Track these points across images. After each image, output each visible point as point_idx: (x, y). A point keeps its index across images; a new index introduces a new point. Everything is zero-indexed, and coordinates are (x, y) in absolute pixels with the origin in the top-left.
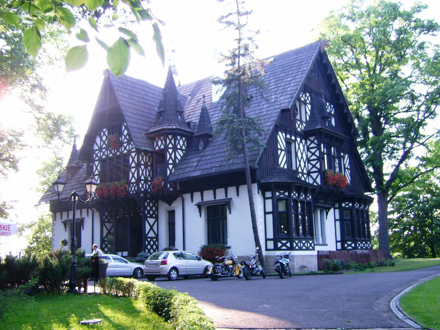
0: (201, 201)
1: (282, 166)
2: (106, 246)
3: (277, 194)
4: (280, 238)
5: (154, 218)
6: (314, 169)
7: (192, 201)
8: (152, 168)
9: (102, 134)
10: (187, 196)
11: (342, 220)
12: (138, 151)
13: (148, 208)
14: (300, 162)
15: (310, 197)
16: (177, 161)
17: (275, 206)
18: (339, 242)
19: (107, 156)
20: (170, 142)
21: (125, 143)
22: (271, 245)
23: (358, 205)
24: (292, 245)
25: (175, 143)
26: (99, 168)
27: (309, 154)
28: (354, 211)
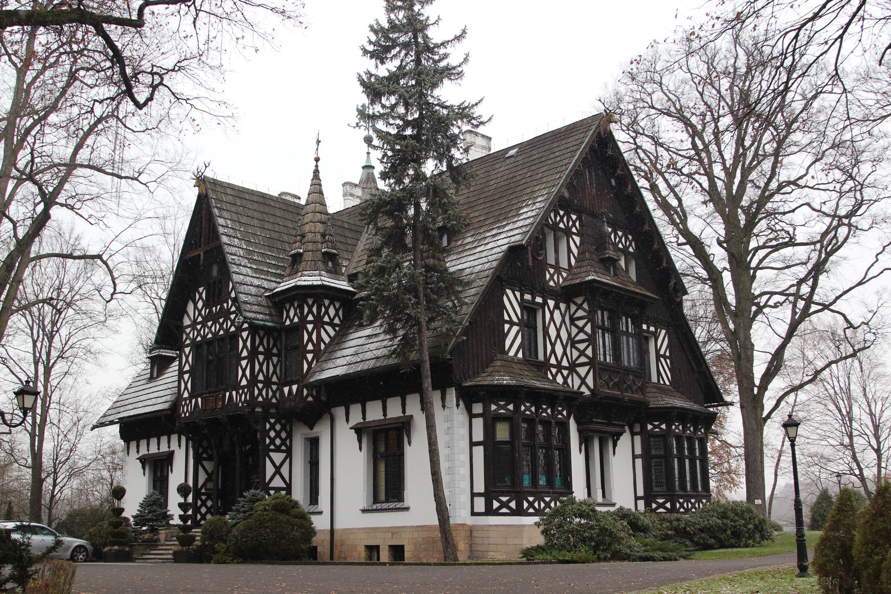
1: (512, 353)
2: (204, 503)
3: (493, 407)
4: (495, 492)
5: (283, 451)
7: (347, 420)
9: (197, 296)
10: (340, 412)
11: (646, 456)
12: (254, 329)
13: (272, 434)
14: (553, 345)
16: (323, 346)
17: (489, 430)
18: (640, 498)
19: (215, 334)
20: (310, 311)
22: (480, 504)
24: (519, 505)
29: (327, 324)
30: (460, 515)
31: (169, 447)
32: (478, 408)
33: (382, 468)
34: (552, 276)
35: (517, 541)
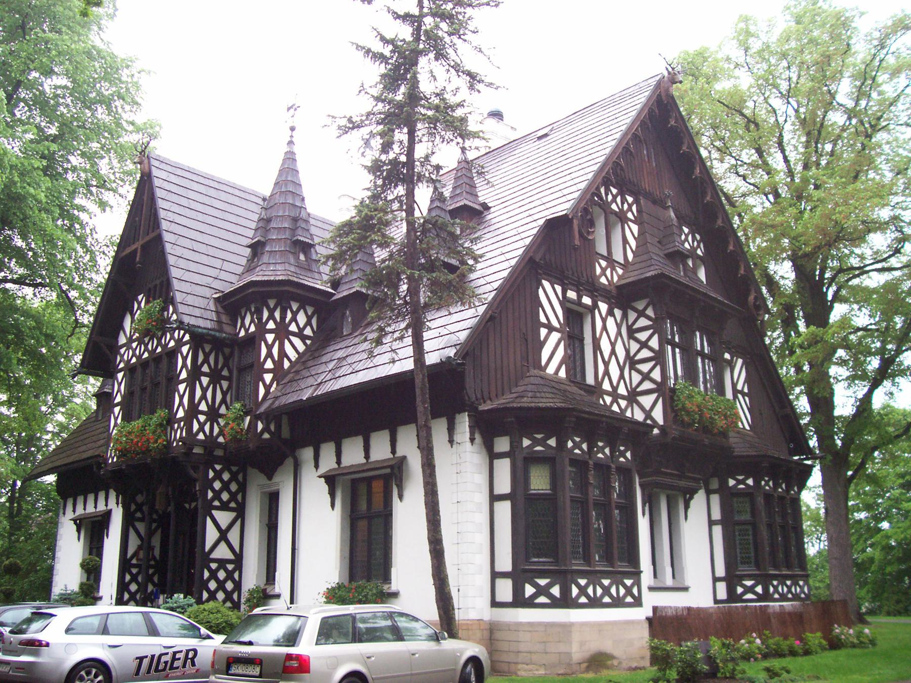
0: (336, 466)
1: (551, 370)
3: (526, 442)
7: (317, 466)
11: (727, 522)
13: (217, 485)
14: (606, 364)
15: (628, 455)
16: (287, 364)
17: (519, 478)
20: (271, 317)
22: (505, 591)
23: (771, 483)
24: (566, 591)
25: (283, 317)
27: (634, 347)
28: (760, 500)
29: (294, 334)
30: (472, 602)
31: (106, 505)
32: (502, 444)
33: (100, 518)
34: (604, 270)
35: (562, 648)
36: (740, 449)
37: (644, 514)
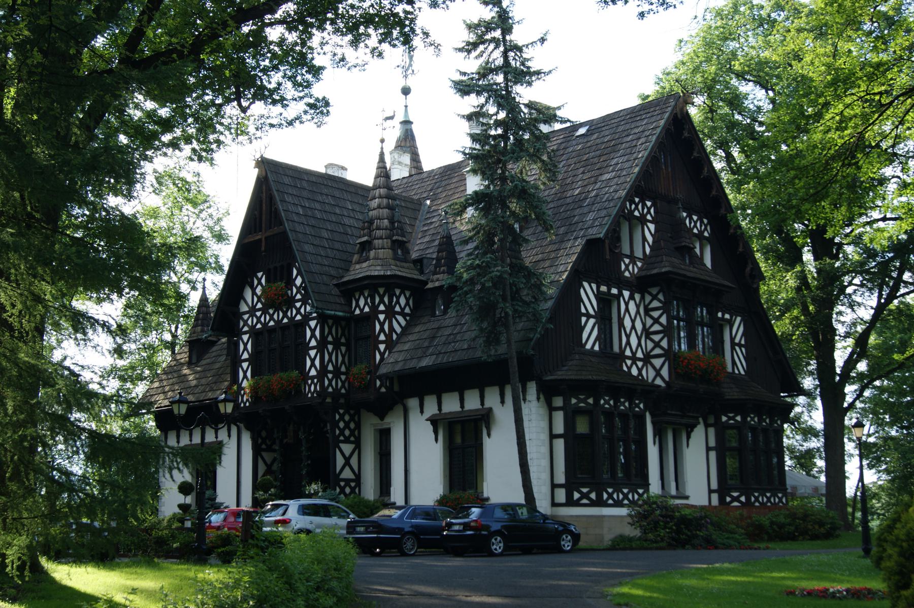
1: (588, 346)
3: (574, 401)
6: (658, 351)
7: (422, 412)
8: (348, 349)
9: (256, 282)
10: (413, 403)
12: (323, 319)
13: (342, 425)
14: (628, 336)
16: (395, 337)
17: (569, 424)
18: (714, 491)
19: (279, 322)
21: (298, 301)
22: (561, 495)
24: (599, 496)
26: (249, 346)
29: (398, 313)
32: (558, 402)
34: (627, 266)
36: (732, 393)
37: (654, 443)
